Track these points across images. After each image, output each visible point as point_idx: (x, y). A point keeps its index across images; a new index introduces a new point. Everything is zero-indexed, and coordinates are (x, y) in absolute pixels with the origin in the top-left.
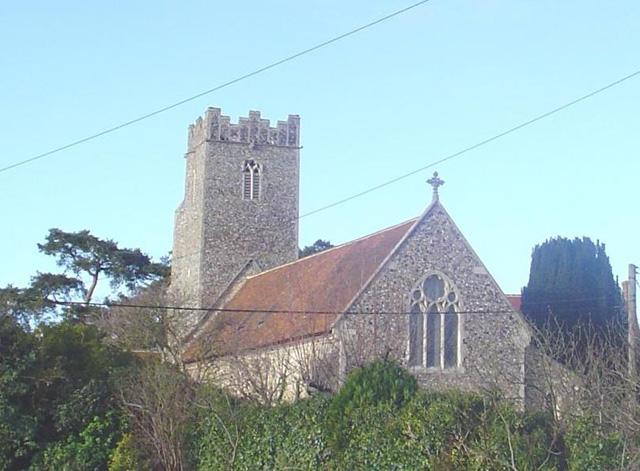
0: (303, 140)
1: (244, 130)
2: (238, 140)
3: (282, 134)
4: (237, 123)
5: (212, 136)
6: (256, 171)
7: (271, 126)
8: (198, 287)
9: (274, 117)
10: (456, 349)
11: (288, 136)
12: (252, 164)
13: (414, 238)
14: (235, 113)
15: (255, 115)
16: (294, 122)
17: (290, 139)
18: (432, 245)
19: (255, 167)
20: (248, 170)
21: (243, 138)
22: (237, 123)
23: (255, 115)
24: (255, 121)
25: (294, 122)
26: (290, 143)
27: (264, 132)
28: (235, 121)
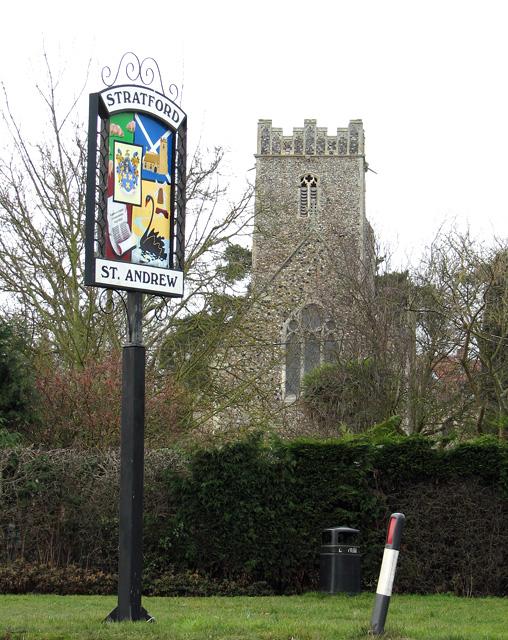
0: (372, 152)
1: (298, 141)
2: (292, 153)
3: (342, 144)
4: (335, 134)
5: (263, 151)
6: (314, 185)
7: (329, 134)
8: (386, 550)
9: (332, 124)
10: (330, 581)
11: (351, 143)
12: (309, 178)
13: (289, 269)
14: (288, 125)
15: (310, 124)
16: (356, 127)
17: (351, 147)
18: (309, 274)
19: (312, 181)
20: (304, 185)
21: (298, 150)
22: (335, 134)
23: (310, 124)
24: (311, 130)
25: (356, 127)
26: (352, 152)
27: (321, 142)
28: (288, 132)
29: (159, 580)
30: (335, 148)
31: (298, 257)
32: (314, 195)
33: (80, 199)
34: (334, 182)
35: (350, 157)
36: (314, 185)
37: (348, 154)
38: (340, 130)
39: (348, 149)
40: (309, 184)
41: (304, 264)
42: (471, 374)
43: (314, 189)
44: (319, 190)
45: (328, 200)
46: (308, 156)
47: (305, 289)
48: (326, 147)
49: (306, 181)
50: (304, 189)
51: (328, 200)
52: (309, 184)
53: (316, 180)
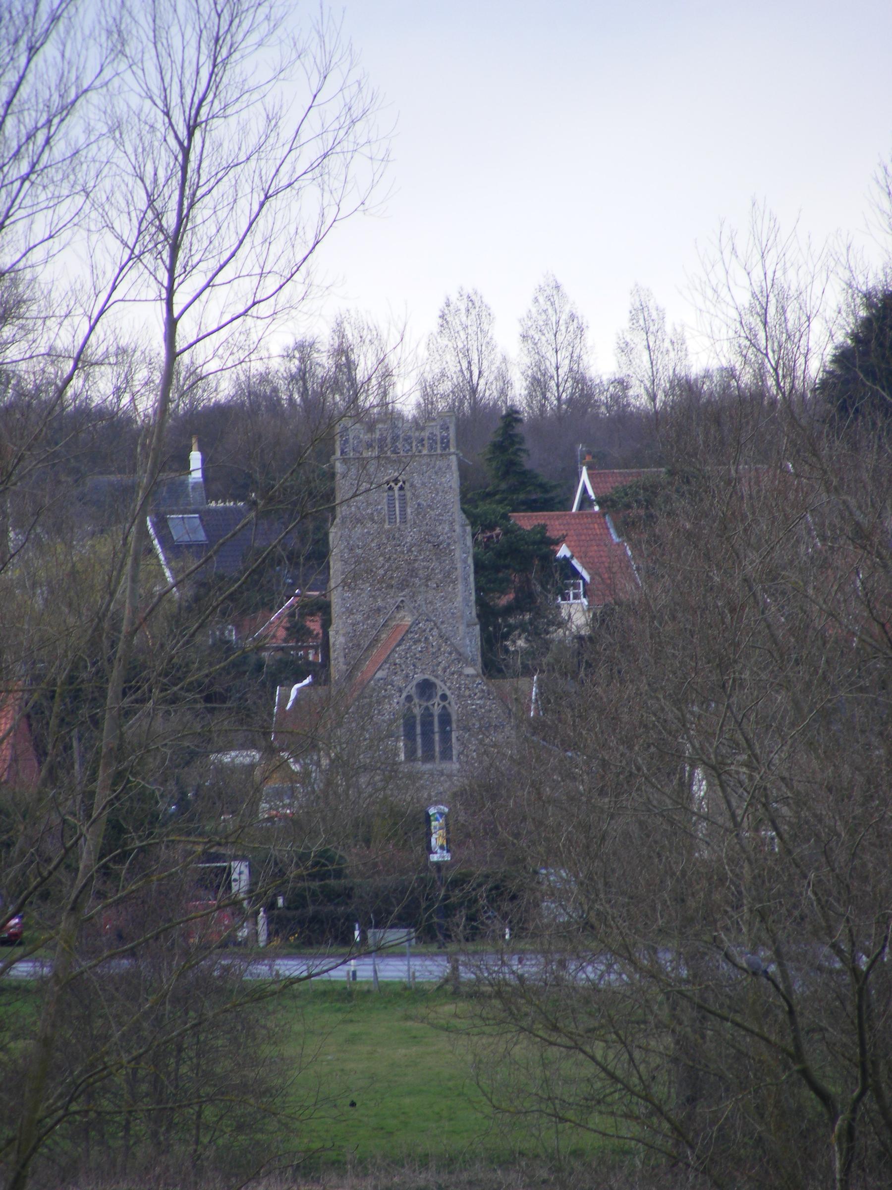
13: (403, 647)
17: (442, 443)
18: (421, 652)
20: (391, 488)
29: (245, 903)
30: (423, 445)
31: (410, 636)
32: (403, 498)
33: (339, 1010)
34: (423, 484)
35: (441, 455)
36: (401, 488)
37: (439, 451)
38: (428, 398)
39: (439, 445)
40: (396, 488)
41: (415, 642)
42: (743, 1033)
43: (402, 493)
44: (409, 495)
45: (419, 505)
46: (394, 456)
47: (418, 665)
48: (414, 444)
49: (393, 484)
50: (391, 493)
51: (419, 505)
52: (396, 488)
53: (404, 482)
